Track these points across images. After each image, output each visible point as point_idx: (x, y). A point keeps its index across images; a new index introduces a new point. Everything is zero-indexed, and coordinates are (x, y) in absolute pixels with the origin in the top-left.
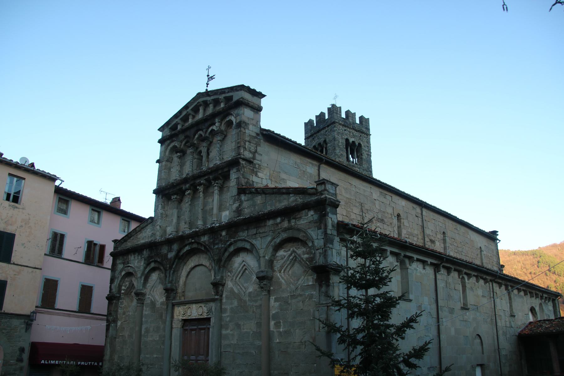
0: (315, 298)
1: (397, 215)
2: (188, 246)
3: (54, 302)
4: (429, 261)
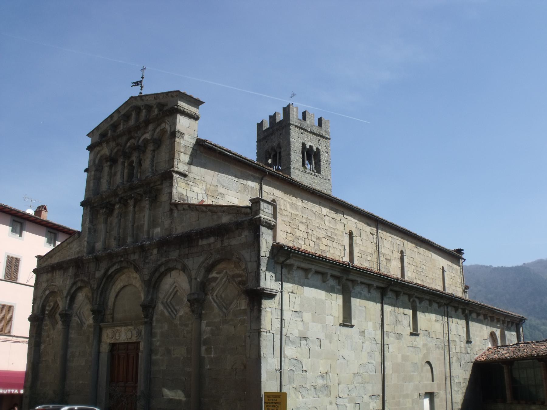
0: (247, 324)
1: (349, 232)
2: (117, 265)
3: (17, 278)
4: (375, 284)
